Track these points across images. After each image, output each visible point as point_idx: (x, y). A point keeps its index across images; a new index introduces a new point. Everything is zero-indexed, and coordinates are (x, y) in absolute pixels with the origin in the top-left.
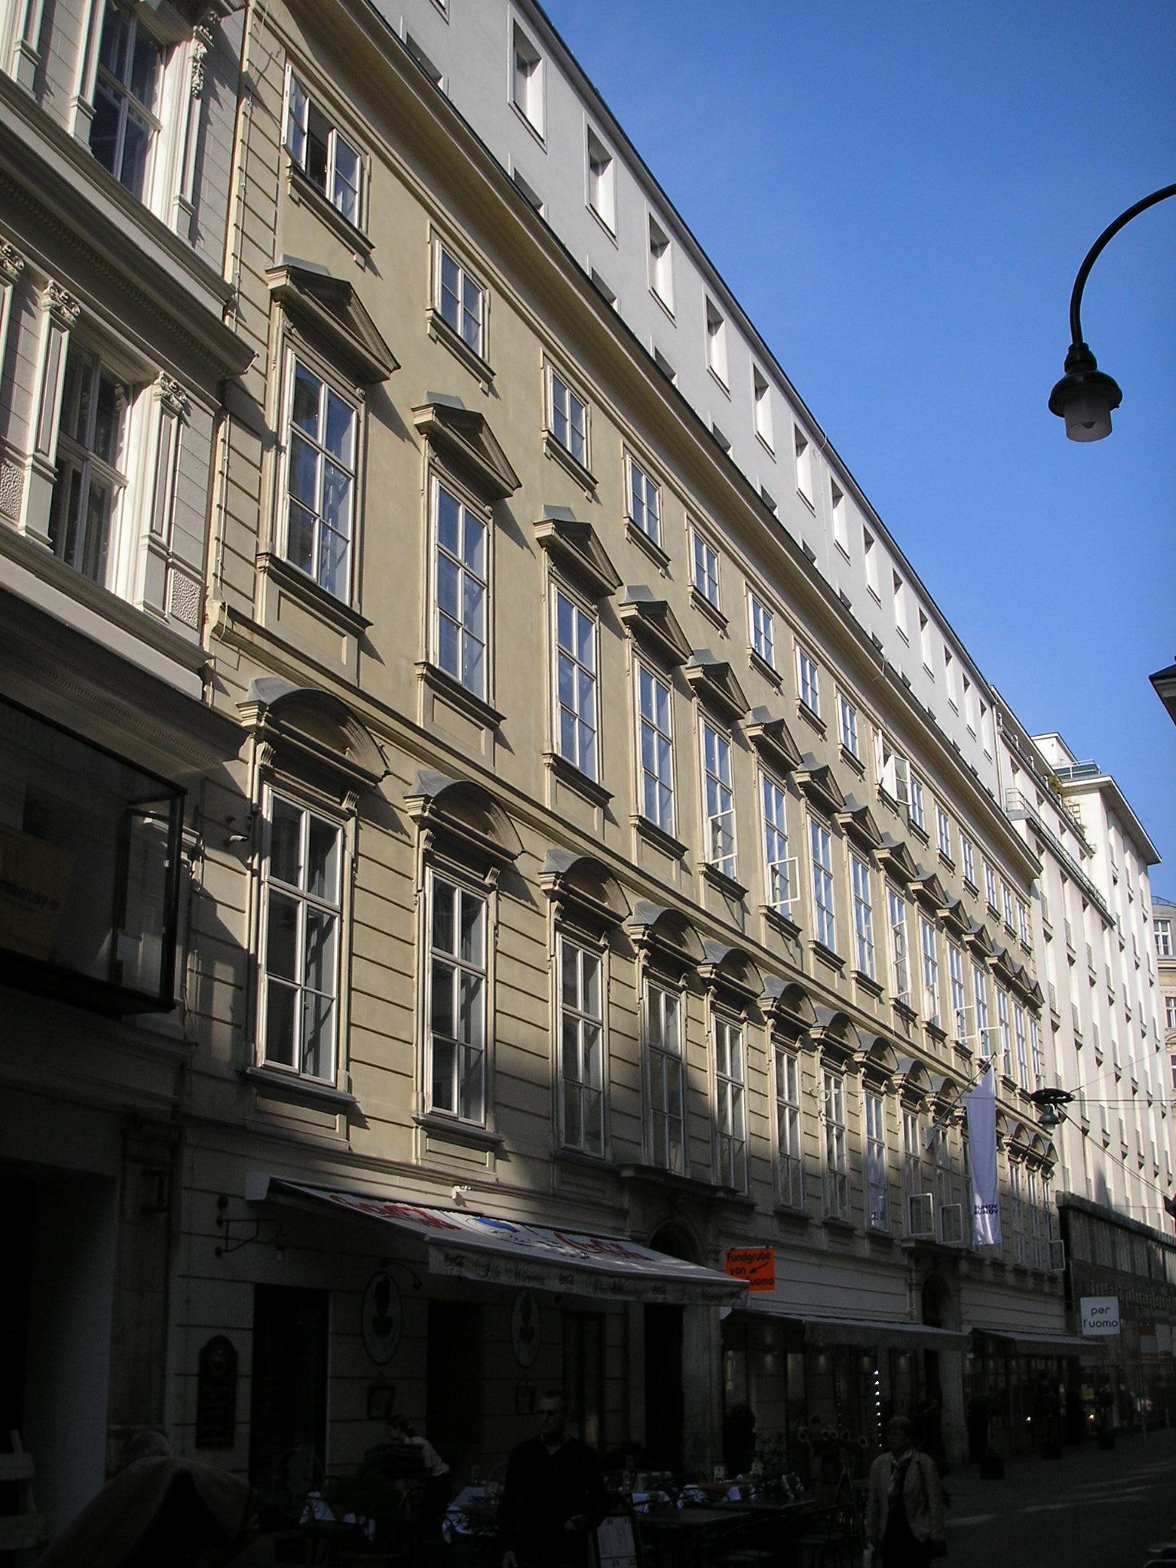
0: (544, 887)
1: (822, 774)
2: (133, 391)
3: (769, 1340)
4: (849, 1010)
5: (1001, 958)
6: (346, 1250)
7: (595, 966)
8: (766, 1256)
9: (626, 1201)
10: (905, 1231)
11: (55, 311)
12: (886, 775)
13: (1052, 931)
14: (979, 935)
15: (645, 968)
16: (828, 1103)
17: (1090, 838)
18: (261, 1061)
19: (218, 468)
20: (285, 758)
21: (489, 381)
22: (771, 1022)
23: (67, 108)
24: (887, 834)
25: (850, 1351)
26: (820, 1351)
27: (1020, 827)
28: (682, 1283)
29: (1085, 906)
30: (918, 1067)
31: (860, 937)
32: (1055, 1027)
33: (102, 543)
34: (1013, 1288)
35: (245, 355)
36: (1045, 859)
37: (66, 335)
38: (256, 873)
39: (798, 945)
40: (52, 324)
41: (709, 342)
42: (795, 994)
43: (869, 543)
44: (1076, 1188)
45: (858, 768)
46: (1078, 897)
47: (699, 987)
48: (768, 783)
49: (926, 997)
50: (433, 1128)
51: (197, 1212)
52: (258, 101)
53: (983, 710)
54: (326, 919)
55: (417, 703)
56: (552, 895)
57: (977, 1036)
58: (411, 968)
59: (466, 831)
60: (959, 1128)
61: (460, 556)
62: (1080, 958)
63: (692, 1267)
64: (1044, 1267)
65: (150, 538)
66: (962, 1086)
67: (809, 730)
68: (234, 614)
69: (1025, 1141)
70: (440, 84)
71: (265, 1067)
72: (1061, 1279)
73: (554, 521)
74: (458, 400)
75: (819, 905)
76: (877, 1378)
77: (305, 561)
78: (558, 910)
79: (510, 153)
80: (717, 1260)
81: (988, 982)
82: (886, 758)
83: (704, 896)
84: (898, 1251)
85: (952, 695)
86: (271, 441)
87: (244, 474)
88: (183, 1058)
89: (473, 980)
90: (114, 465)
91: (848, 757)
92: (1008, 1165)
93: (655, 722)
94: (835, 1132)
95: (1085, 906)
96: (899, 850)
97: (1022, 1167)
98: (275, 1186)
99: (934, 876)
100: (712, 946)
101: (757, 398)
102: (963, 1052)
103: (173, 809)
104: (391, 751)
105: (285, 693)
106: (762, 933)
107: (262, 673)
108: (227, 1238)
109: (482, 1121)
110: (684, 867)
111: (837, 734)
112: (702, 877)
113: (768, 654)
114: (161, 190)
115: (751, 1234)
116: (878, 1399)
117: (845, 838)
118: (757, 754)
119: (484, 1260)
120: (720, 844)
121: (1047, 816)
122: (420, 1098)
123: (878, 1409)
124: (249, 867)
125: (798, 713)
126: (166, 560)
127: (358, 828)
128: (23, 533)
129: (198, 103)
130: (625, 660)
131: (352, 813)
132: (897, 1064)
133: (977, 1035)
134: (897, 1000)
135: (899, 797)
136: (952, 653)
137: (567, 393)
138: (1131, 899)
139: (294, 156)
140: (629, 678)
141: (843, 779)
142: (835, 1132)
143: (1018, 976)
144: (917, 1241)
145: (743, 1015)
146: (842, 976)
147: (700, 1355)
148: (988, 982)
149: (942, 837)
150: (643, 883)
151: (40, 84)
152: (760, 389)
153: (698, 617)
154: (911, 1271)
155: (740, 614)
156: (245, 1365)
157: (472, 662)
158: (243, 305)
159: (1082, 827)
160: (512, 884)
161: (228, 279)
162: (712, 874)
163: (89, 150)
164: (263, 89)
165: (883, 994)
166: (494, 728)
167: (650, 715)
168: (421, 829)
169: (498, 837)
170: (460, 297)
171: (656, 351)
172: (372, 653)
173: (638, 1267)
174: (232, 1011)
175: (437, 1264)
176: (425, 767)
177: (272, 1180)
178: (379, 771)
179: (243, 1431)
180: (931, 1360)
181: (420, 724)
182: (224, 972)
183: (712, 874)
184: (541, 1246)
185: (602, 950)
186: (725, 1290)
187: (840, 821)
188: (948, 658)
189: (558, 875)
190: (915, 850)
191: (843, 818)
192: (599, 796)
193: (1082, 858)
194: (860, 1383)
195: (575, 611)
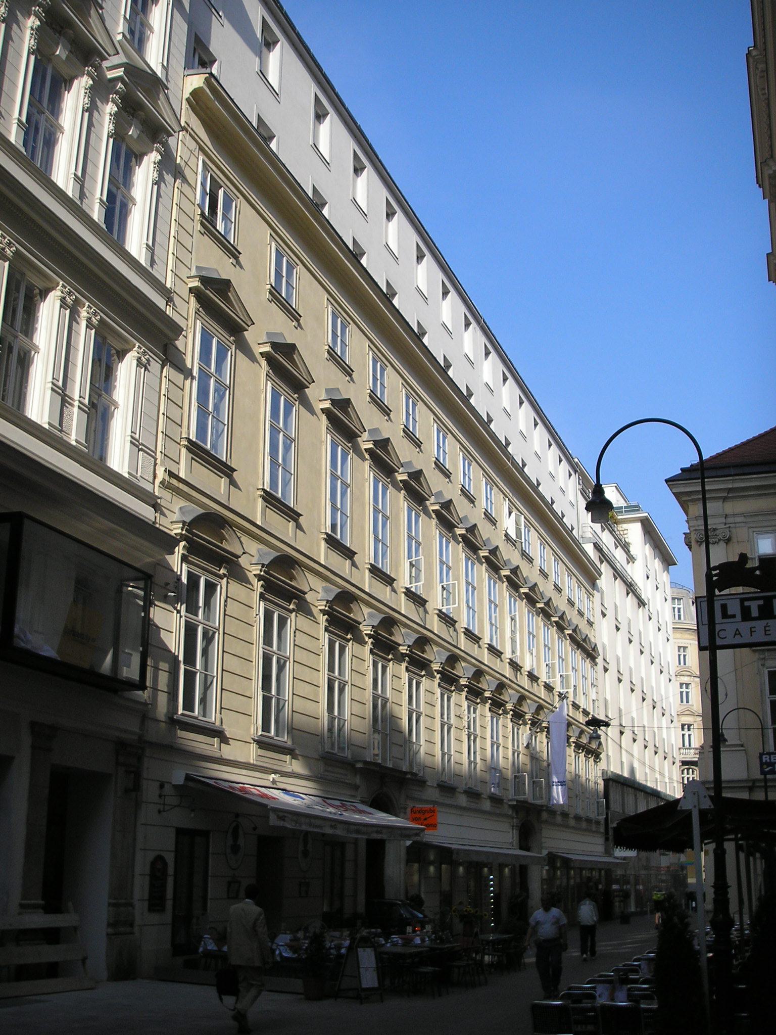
0: (255, 572)
1: (447, 505)
2: (44, 294)
3: (432, 858)
4: (483, 666)
5: (547, 604)
6: (219, 809)
7: (286, 623)
8: (433, 811)
9: (358, 780)
10: (510, 795)
11: (89, 320)
12: (509, 524)
13: (607, 613)
14: (547, 604)
15: (371, 650)
16: (469, 723)
17: (633, 550)
18: (180, 711)
19: (163, 392)
20: (195, 549)
21: (298, 321)
22: (438, 676)
23: (11, 125)
24: (509, 560)
25: (477, 866)
26: (460, 864)
27: (589, 548)
28: (391, 828)
29: (628, 594)
30: (522, 699)
31: (491, 623)
32: (606, 670)
33: (24, 390)
34: (573, 828)
35: (178, 330)
36: (604, 568)
37: (93, 331)
38: (179, 612)
39: (455, 630)
40: (87, 327)
41: (387, 227)
42: (453, 659)
43: (487, 354)
44: (615, 769)
45: (493, 522)
46: (624, 589)
47: (400, 658)
48: (441, 536)
49: (528, 657)
50: (263, 744)
51: (150, 791)
52: (185, 180)
53: (570, 475)
54: (211, 633)
55: (258, 511)
56: (324, 612)
57: (558, 679)
58: (251, 655)
59: (282, 583)
60: (545, 733)
61: (213, 370)
62: (624, 627)
63: (394, 818)
64: (592, 816)
65: (53, 383)
66: (548, 709)
67: (466, 501)
68: (171, 474)
69: (584, 740)
70: (273, 145)
71: (182, 714)
72: (603, 822)
73: (331, 399)
74: (282, 334)
75: (468, 606)
76: (492, 880)
77: (335, 533)
78: (327, 620)
79: (307, 176)
80: (405, 813)
81: (566, 645)
82: (510, 513)
83: (404, 606)
84: (506, 806)
85: (551, 468)
86: (188, 374)
87: (175, 394)
88: (145, 713)
89: (282, 661)
90: (32, 339)
91: (465, 493)
92: (573, 754)
93: (380, 507)
94: (472, 738)
95: (628, 594)
96: (515, 570)
97: (582, 755)
98: (188, 778)
99: (536, 584)
100: (408, 634)
101: (466, 330)
102: (549, 688)
103: (146, 585)
104: (244, 539)
105: (195, 515)
106: (435, 625)
107: (182, 503)
108: (164, 804)
109: (285, 738)
110: (394, 590)
111: (482, 503)
112: (403, 595)
113: (444, 459)
114: (136, 241)
115: (425, 798)
116: (492, 892)
117: (484, 565)
118: (436, 520)
119: (295, 818)
120: (413, 574)
121: (607, 539)
122: (255, 727)
123: (492, 898)
124: (175, 608)
125: (460, 492)
126: (137, 446)
127: (228, 582)
128: (74, 443)
129: (87, 115)
130: (366, 471)
131: (225, 575)
132: (509, 698)
133: (558, 676)
134: (510, 659)
135: (517, 537)
136: (563, 458)
137: (339, 320)
138: (657, 588)
139: (201, 206)
140: (367, 484)
141: (485, 530)
142: (472, 738)
143: (584, 640)
144: (517, 801)
145: (423, 673)
146: (480, 647)
147: (395, 868)
148: (566, 645)
149: (543, 561)
150: (372, 601)
151: (82, 195)
152: (420, 257)
153: (406, 442)
154: (513, 818)
155: (429, 437)
156: (171, 870)
157: (218, 435)
158: (176, 299)
159: (628, 544)
160: (304, 608)
161: (168, 285)
162: (409, 593)
163: (104, 227)
164: (188, 173)
165: (457, 625)
166: (296, 521)
167: (378, 504)
168: (259, 580)
169: (298, 584)
170: (284, 274)
171: (506, 438)
172: (236, 486)
173: (366, 819)
174: (168, 686)
175: (273, 820)
176: (261, 546)
177: (187, 774)
178: (239, 553)
179: (169, 904)
180: (522, 872)
181: (259, 523)
182: (164, 666)
183: (409, 593)
184: (330, 811)
185: (348, 641)
186: (415, 832)
187: (458, 533)
188: (550, 445)
189: (328, 601)
190: (526, 570)
191: (483, 553)
192: (349, 554)
193: (628, 563)
194: (482, 882)
195: (282, 398)
